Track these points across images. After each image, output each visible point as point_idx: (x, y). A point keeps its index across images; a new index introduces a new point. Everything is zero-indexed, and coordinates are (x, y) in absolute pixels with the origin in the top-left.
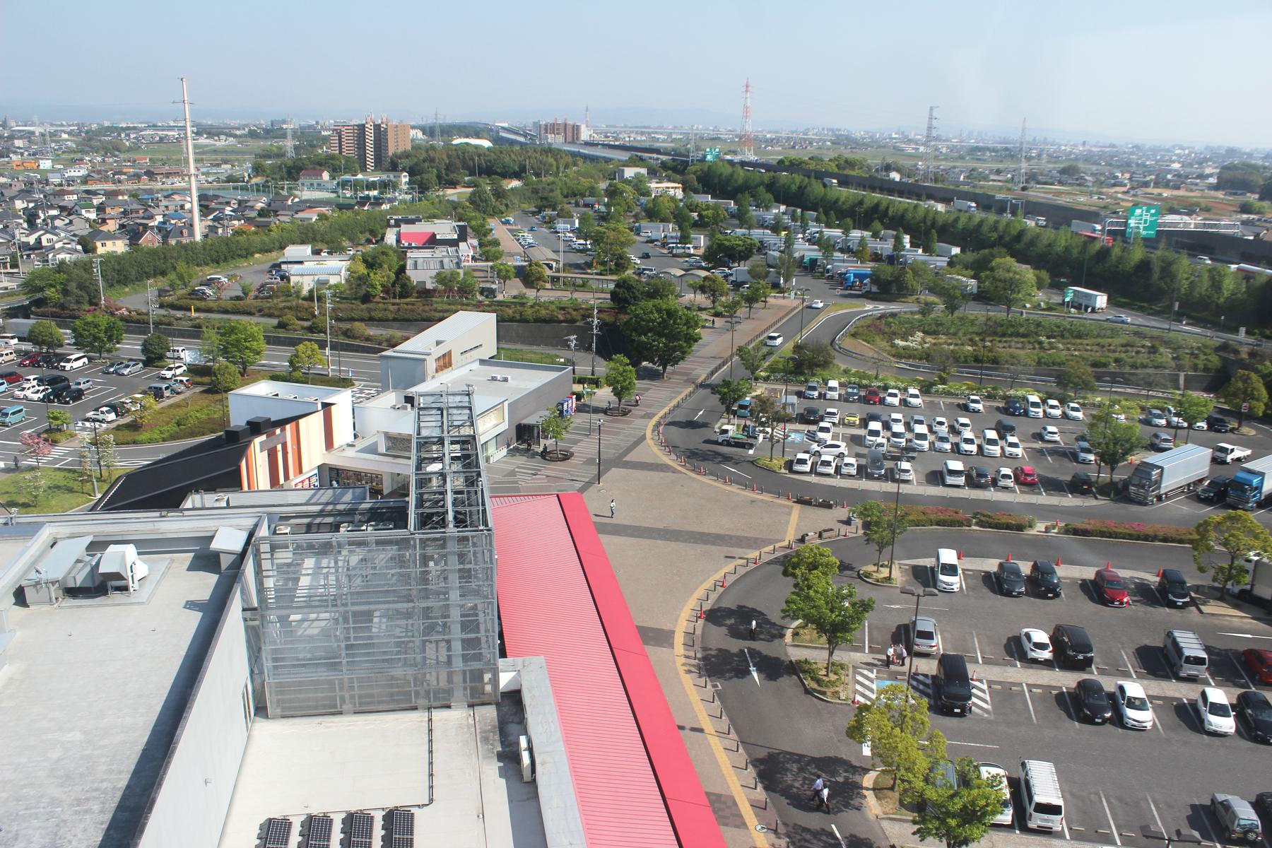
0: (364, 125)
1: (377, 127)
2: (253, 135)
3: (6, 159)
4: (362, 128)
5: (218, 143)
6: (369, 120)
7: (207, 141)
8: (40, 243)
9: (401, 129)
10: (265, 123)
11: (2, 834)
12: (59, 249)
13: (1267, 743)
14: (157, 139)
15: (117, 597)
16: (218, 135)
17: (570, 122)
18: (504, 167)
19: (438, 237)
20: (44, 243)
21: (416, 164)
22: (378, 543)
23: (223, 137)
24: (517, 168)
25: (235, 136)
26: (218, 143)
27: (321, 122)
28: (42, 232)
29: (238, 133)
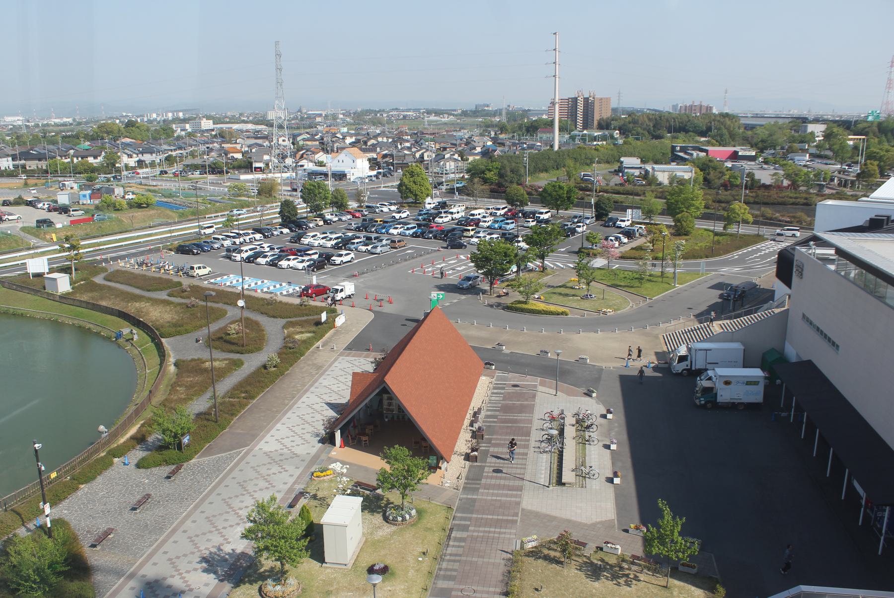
0: (577, 98)
1: (586, 100)
2: (465, 113)
3: (315, 129)
4: (575, 100)
5: (443, 120)
6: (580, 94)
7: (436, 118)
8: (423, 158)
9: (605, 101)
10: (473, 108)
11: (3, 226)
12: (448, 159)
13: (2, 233)
14: (402, 117)
15: (807, 315)
16: (442, 114)
17: (705, 104)
18: (695, 127)
19: (740, 154)
20: (426, 158)
21: (624, 125)
22: (648, 280)
23: (446, 116)
24: (704, 128)
25: (453, 115)
26: (443, 120)
27: (512, 106)
28: (424, 150)
29: (455, 113)
